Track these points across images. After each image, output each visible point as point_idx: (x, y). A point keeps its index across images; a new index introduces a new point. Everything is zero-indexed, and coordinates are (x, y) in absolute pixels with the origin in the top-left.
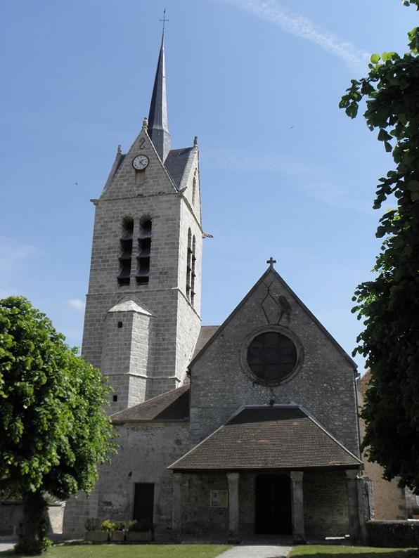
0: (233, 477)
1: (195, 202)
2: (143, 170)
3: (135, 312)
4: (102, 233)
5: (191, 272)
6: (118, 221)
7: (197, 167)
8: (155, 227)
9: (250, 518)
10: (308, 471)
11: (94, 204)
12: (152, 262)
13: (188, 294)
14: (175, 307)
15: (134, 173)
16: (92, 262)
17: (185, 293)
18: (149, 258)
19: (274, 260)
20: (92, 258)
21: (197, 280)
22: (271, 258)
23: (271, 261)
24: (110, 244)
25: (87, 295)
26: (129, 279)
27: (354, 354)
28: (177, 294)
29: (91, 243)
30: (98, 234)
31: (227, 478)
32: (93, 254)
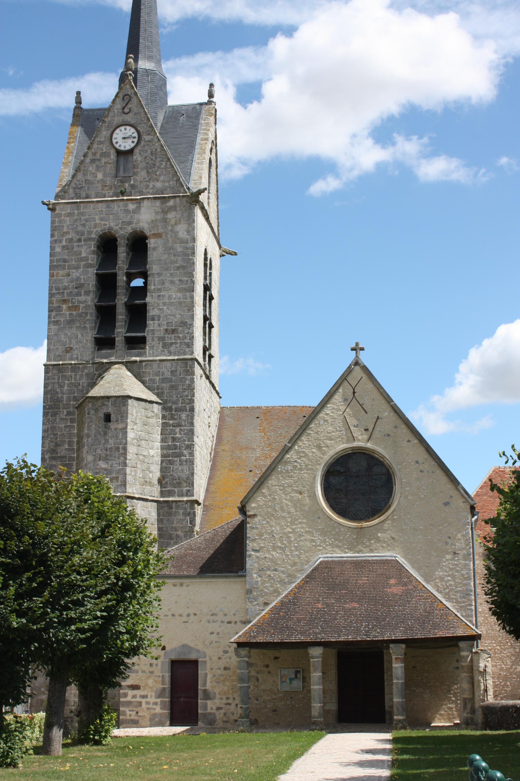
0: (316, 652)
1: (211, 204)
2: (131, 152)
3: (130, 397)
4: (65, 261)
5: (207, 322)
6: (90, 239)
7: (214, 139)
8: (155, 253)
9: (333, 706)
10: (409, 643)
11: (49, 209)
12: (152, 312)
13: (204, 358)
14: (191, 388)
15: (113, 156)
16: (50, 310)
17: (201, 360)
18: (145, 305)
19: (360, 346)
20: (50, 302)
21: (214, 331)
22: (357, 344)
23: (357, 349)
24: (78, 278)
25: (45, 365)
26: (114, 339)
27: (476, 554)
28: (192, 367)
29: (48, 277)
30: (58, 261)
31: (308, 654)
32: (51, 295)
